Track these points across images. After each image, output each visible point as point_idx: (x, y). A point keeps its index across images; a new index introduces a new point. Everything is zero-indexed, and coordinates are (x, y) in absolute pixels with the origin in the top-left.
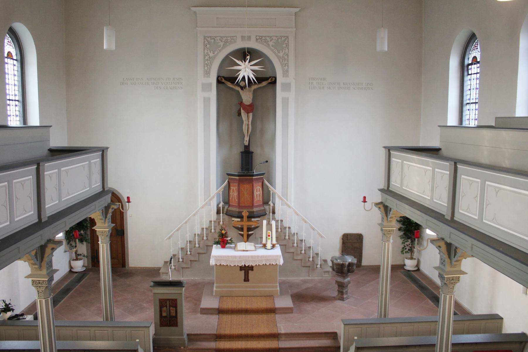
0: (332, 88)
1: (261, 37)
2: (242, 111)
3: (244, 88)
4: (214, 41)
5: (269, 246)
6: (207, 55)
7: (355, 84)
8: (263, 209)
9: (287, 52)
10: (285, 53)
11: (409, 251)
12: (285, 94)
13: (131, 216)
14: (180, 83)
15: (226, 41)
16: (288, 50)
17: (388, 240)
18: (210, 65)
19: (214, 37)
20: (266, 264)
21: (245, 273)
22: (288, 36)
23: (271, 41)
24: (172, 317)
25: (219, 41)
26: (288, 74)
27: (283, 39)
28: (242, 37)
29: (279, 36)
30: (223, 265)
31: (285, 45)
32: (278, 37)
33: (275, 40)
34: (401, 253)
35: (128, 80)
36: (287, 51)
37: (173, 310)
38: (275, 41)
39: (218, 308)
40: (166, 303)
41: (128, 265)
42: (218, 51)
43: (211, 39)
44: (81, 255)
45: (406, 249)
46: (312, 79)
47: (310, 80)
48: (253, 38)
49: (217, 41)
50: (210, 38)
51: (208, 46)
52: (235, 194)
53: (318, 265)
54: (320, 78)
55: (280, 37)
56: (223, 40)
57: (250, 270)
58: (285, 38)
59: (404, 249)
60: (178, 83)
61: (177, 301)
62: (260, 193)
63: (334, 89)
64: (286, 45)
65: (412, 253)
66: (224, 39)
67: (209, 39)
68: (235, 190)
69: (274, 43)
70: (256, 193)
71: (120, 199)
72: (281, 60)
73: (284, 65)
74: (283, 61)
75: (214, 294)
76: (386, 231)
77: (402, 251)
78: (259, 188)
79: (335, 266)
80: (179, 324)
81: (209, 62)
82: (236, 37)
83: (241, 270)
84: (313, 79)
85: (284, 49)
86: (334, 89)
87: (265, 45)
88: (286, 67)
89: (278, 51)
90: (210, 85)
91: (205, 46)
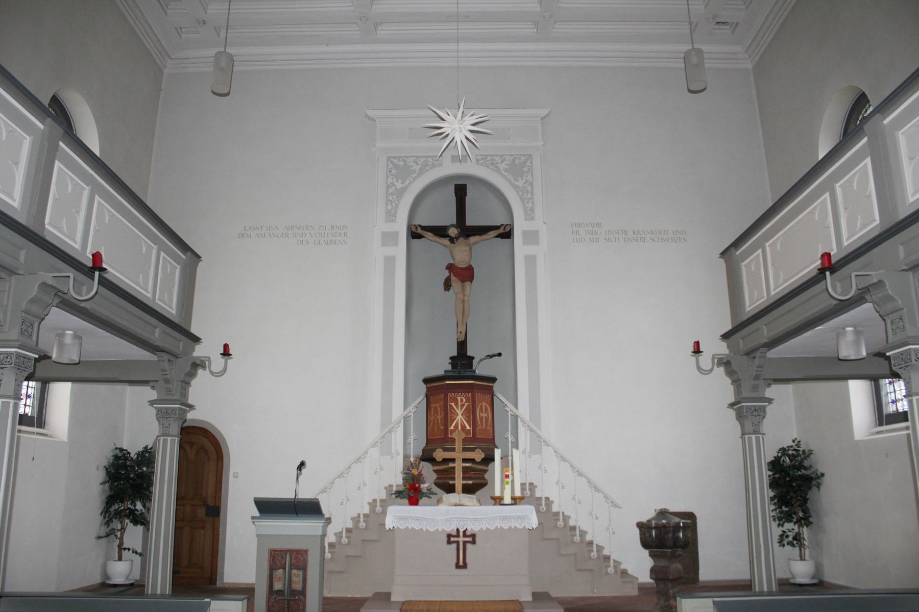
3: (455, 240)
5: (507, 500)
6: (392, 186)
7: (654, 232)
9: (531, 180)
10: (527, 181)
11: (795, 542)
12: (530, 250)
13: (237, 477)
15: (424, 164)
16: (532, 176)
17: (755, 430)
18: (396, 202)
24: (293, 593)
26: (533, 215)
30: (412, 528)
32: (514, 157)
33: (509, 160)
34: (779, 544)
35: (252, 229)
37: (297, 574)
38: (509, 162)
40: (284, 558)
41: (222, 578)
42: (411, 180)
44: (129, 549)
45: (787, 536)
47: (574, 227)
51: (394, 171)
53: (609, 566)
54: (591, 224)
56: (420, 162)
58: (525, 158)
59: (784, 537)
60: (340, 235)
64: (528, 169)
65: (803, 549)
66: (422, 160)
67: (396, 161)
68: (439, 409)
69: (507, 165)
71: (219, 445)
72: (521, 193)
74: (523, 195)
76: (748, 410)
77: (780, 540)
78: (485, 406)
81: (394, 197)
85: (526, 174)
87: (492, 169)
88: (530, 205)
90: (396, 234)
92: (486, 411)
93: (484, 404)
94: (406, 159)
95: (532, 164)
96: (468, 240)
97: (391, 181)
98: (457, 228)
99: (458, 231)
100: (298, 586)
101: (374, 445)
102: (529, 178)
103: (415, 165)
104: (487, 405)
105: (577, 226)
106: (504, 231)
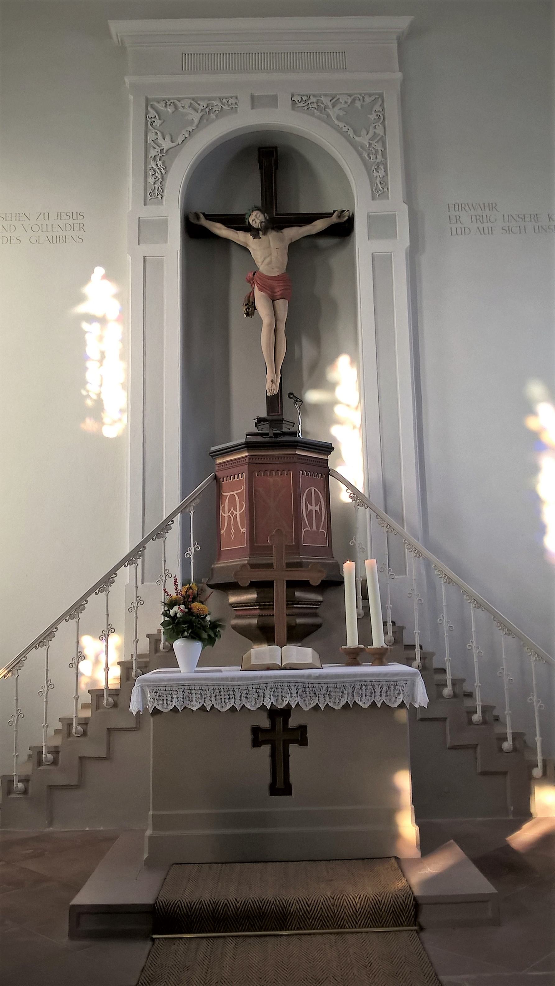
1: (305, 98)
4: (173, 109)
9: (382, 134)
14: (77, 228)
18: (163, 172)
20: (355, 703)
21: (273, 755)
23: (334, 107)
25: (190, 111)
27: (368, 100)
28: (253, 97)
31: (373, 116)
33: (346, 102)
38: (346, 106)
39: (153, 906)
43: (166, 106)
48: (284, 100)
49: (184, 111)
50: (163, 104)
51: (158, 122)
52: (238, 513)
55: (361, 95)
56: (201, 108)
57: (294, 742)
60: (72, 227)
62: (320, 509)
63: (523, 231)
66: (204, 104)
67: (160, 107)
82: (236, 98)
83: (256, 743)
86: (523, 231)
87: (319, 118)
88: (381, 173)
89: (355, 132)
91: (149, 123)
92: (318, 501)
93: (313, 488)
94: (177, 102)
95: (383, 109)
97: (154, 137)
98: (263, 212)
99: (265, 218)
102: (380, 131)
104: (316, 490)
105: (457, 209)
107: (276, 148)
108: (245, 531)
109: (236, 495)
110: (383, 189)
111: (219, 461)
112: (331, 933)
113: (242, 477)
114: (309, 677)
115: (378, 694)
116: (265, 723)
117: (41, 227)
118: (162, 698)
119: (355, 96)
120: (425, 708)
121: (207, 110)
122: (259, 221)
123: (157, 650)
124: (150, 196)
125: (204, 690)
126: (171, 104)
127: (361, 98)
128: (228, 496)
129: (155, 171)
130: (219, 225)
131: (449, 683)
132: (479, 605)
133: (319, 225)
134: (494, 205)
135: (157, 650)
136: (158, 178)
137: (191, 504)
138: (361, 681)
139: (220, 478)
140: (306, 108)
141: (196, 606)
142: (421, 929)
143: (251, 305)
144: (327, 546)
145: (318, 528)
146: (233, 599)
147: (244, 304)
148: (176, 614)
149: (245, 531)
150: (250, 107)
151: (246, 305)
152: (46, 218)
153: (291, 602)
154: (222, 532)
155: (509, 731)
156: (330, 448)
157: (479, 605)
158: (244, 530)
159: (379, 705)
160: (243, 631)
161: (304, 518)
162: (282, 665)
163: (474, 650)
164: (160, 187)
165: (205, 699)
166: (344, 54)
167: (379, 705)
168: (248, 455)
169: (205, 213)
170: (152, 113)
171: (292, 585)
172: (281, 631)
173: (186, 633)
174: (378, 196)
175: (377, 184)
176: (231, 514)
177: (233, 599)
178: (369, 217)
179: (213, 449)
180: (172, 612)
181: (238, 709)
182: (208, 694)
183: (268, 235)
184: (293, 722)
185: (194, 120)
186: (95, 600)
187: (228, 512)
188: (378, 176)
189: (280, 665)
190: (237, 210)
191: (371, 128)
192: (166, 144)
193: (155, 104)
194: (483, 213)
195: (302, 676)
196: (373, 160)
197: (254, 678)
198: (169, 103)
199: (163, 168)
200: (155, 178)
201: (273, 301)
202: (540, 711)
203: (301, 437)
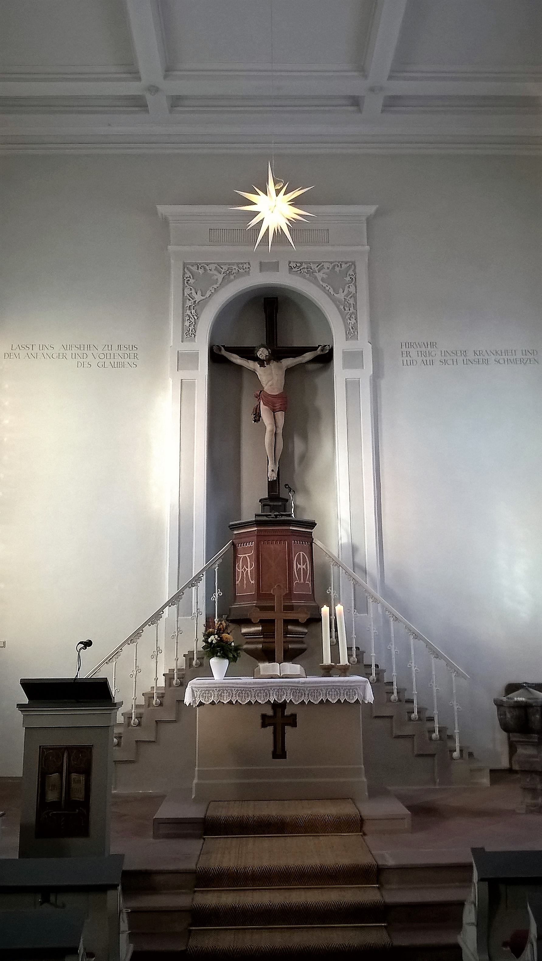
0: (450, 362)
2: (263, 408)
4: (203, 271)
7: (500, 352)
8: (313, 604)
9: (354, 292)
12: (352, 374)
16: (356, 287)
18: (196, 318)
19: (205, 263)
22: (355, 262)
25: (216, 273)
29: (336, 261)
31: (348, 279)
33: (328, 268)
36: (352, 289)
39: (204, 819)
43: (198, 269)
46: (407, 344)
49: (211, 272)
50: (196, 267)
51: (192, 281)
52: (249, 570)
53: (455, 751)
56: (223, 271)
61: (91, 752)
62: (306, 567)
63: (455, 363)
66: (225, 268)
67: (194, 269)
70: (297, 565)
73: (348, 316)
75: (193, 797)
79: (510, 712)
80: (93, 829)
83: (264, 725)
84: (410, 345)
86: (455, 363)
88: (353, 321)
89: (334, 291)
90: (194, 357)
91: (185, 282)
93: (301, 553)
95: (355, 273)
96: (281, 362)
97: (189, 292)
99: (269, 353)
100: (79, 796)
101: (170, 603)
103: (217, 274)
104: (304, 554)
106: (322, 353)
107: (277, 298)
108: (254, 583)
109: (248, 558)
110: (354, 332)
111: (236, 532)
112: (310, 836)
113: (252, 544)
114: (298, 682)
115: (342, 694)
116: (270, 712)
117: (106, 356)
118: (204, 695)
119: (334, 263)
120: (371, 703)
121: (228, 272)
122: (265, 355)
123: (191, 665)
124: (186, 335)
125: (232, 690)
126: (202, 268)
127: (339, 265)
128: (242, 558)
129: (190, 317)
130: (235, 356)
131: (395, 691)
132: (417, 637)
133: (308, 356)
134: (434, 344)
135: (191, 665)
136: (192, 322)
137: (216, 562)
138: (331, 686)
139: (236, 544)
140: (299, 272)
141: (225, 635)
142: (365, 834)
143: (258, 415)
144: (311, 593)
145: (304, 581)
146: (244, 630)
147: (253, 414)
148: (212, 641)
149: (254, 583)
150: (259, 271)
151: (254, 415)
152: (110, 348)
153: (286, 632)
154: (237, 582)
155: (437, 725)
156: (313, 524)
157: (417, 637)
158: (253, 582)
159: (342, 702)
160: (252, 653)
161: (295, 575)
162: (280, 675)
163: (413, 668)
164: (194, 329)
165: (232, 696)
166: (327, 231)
167: (342, 702)
168: (257, 530)
169: (225, 346)
170: (188, 274)
171: (287, 622)
172: (279, 653)
173: (219, 654)
174: (351, 337)
175: (350, 329)
176: (244, 570)
177: (244, 630)
178: (344, 352)
179: (231, 523)
180: (210, 640)
181: (253, 703)
182: (234, 693)
183: (271, 364)
184: (287, 712)
185: (218, 280)
186: (149, 630)
187: (242, 569)
188: (351, 323)
189: (279, 675)
190: (247, 343)
191: (346, 287)
192: (198, 297)
193: (190, 267)
194: (426, 349)
195: (295, 682)
196: (347, 311)
197: (265, 683)
198: (200, 267)
199: (195, 315)
200: (190, 323)
201: (274, 413)
202: (458, 711)
203: (293, 517)
